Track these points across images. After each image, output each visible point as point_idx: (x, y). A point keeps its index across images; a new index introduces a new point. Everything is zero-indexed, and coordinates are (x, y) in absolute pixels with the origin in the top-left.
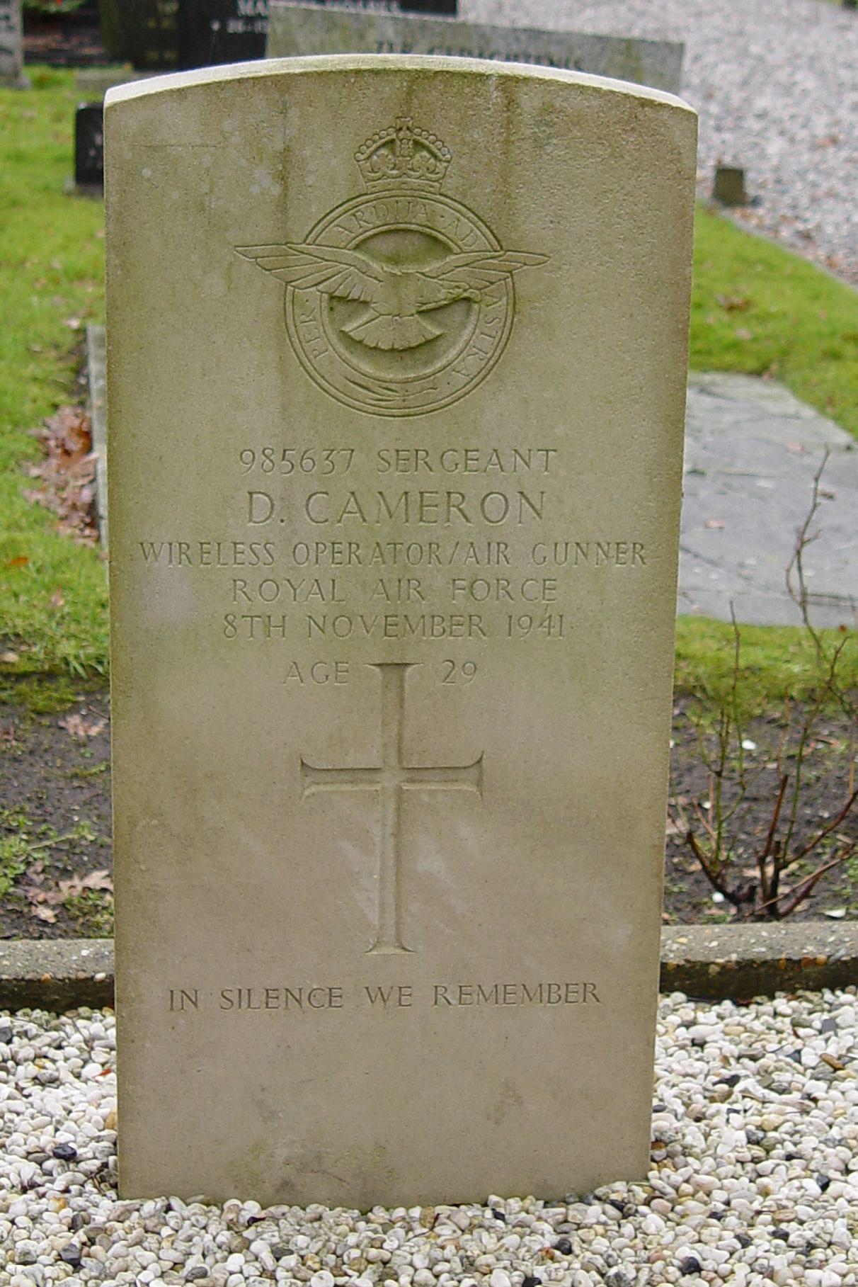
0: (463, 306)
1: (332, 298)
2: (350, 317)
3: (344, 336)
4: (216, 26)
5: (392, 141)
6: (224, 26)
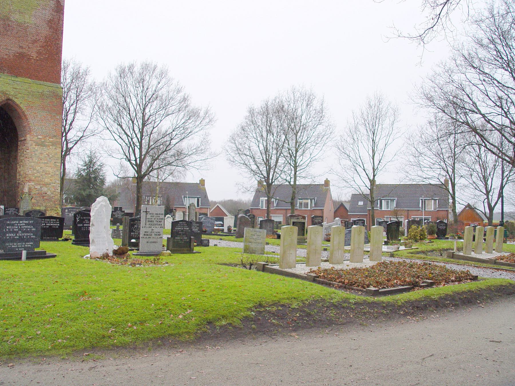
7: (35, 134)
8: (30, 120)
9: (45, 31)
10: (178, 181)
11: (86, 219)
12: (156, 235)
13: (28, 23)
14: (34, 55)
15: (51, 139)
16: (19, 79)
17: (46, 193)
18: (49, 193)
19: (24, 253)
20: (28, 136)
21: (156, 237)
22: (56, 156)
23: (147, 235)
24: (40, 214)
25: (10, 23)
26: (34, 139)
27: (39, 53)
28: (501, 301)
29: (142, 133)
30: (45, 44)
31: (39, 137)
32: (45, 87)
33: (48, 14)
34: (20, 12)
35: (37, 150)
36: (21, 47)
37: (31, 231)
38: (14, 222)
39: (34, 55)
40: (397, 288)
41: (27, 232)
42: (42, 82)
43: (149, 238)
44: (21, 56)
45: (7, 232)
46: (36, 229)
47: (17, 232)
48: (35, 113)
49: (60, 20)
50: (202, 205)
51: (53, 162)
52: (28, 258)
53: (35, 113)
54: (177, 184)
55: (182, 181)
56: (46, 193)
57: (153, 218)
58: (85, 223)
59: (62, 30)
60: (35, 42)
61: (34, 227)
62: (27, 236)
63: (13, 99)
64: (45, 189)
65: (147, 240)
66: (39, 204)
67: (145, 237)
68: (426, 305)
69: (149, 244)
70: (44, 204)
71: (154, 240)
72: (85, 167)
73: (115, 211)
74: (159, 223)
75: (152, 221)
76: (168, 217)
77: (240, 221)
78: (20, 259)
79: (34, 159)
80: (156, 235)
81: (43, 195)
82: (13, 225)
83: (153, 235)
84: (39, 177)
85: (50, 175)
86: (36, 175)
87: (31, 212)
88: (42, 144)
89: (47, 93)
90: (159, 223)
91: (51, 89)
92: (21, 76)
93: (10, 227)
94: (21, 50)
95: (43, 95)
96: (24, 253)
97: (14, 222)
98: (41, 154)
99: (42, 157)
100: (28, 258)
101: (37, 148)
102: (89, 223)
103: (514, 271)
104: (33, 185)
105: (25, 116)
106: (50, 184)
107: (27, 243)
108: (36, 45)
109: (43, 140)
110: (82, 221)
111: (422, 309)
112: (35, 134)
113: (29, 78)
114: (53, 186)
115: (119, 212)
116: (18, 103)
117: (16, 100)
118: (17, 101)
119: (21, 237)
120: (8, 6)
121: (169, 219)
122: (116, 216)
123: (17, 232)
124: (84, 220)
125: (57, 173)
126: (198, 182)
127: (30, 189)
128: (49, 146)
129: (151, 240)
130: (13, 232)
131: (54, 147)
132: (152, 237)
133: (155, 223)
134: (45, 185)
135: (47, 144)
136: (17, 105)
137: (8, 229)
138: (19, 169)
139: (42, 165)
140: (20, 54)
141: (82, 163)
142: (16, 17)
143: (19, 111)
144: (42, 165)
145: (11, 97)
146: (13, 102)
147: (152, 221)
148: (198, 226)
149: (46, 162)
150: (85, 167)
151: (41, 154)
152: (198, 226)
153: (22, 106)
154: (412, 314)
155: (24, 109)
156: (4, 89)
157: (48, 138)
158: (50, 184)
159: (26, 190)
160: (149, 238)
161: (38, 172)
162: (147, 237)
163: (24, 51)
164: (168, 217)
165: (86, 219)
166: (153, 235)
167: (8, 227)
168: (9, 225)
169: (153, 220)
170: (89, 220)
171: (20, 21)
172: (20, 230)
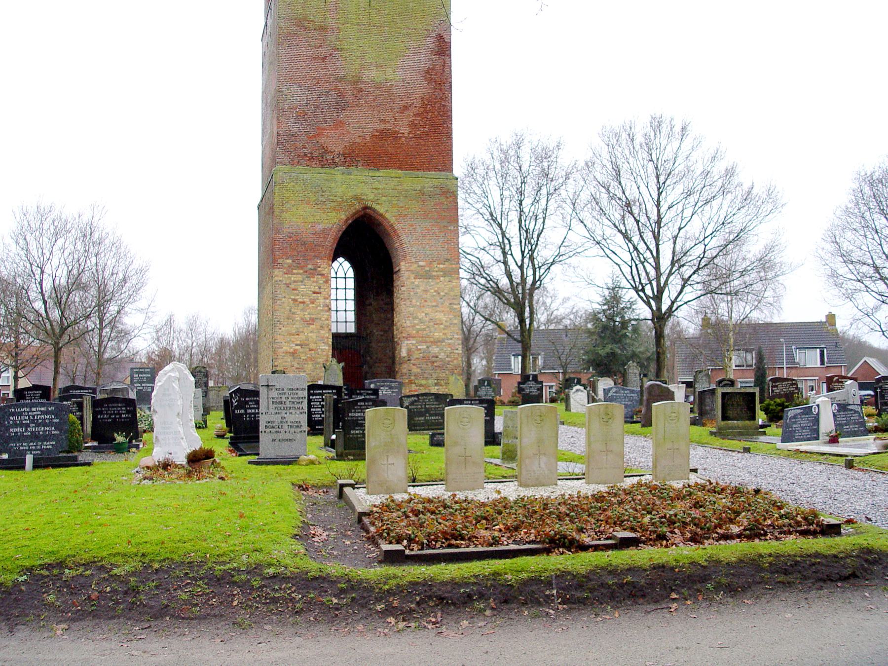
7: (413, 260)
8: (404, 237)
9: (421, 89)
10: (768, 320)
11: (251, 401)
12: (291, 426)
13: (391, 80)
14: (405, 130)
15: (442, 266)
16: (382, 173)
17: (437, 357)
18: (442, 356)
19: (29, 459)
20: (402, 264)
21: (292, 430)
22: (452, 293)
25: (362, 86)
26: (412, 268)
27: (413, 125)
28: (796, 602)
29: (657, 238)
30: (422, 110)
31: (421, 263)
32: (427, 180)
33: (424, 60)
34: (377, 66)
35: (418, 286)
36: (383, 121)
37: (51, 424)
38: (22, 410)
39: (405, 130)
40: (496, 549)
41: (45, 424)
42: (420, 173)
43: (277, 432)
44: (383, 135)
45: (11, 426)
46: (61, 419)
47: (27, 426)
48: (412, 225)
49: (446, 66)
50: (829, 362)
51: (447, 303)
52: (35, 467)
53: (412, 225)
54: (768, 325)
55: (776, 320)
56: (437, 357)
57: (284, 397)
58: (250, 408)
59: (451, 83)
60: (406, 108)
61: (56, 417)
62: (45, 431)
63: (374, 206)
64: (435, 350)
65: (274, 436)
66: (426, 375)
67: (268, 430)
68: (470, 596)
69: (277, 443)
70: (434, 376)
72: (606, 307)
73: (523, 383)
74: (297, 406)
76: (577, 390)
77: (649, 393)
78: (21, 466)
79: (414, 301)
80: (291, 426)
81: (431, 360)
82: (21, 414)
84: (424, 330)
85: (442, 326)
86: (418, 327)
88: (426, 276)
89: (429, 189)
90: (297, 406)
91: (435, 182)
92: (387, 167)
93: (16, 418)
94: (382, 126)
95: (423, 195)
96: (29, 459)
97: (22, 410)
98: (426, 291)
99: (428, 296)
100: (35, 467)
101: (417, 282)
102: (258, 408)
104: (413, 345)
105: (395, 231)
106: (443, 341)
107: (45, 443)
108: (407, 113)
109: (427, 269)
110: (241, 405)
111: (454, 604)
112: (413, 260)
113: (400, 168)
114: (450, 344)
115: (531, 384)
116: (382, 211)
117: (377, 207)
118: (381, 209)
119: (35, 432)
120: (358, 60)
121: (579, 393)
122: (527, 391)
123: (27, 426)
124: (247, 402)
125: (455, 321)
126: (824, 320)
127: (409, 351)
128: (438, 277)
130: (21, 425)
131: (447, 279)
132: (282, 431)
133: (288, 405)
134: (436, 342)
135: (435, 274)
136: (381, 215)
137: (13, 420)
138: (396, 320)
139: (428, 310)
140: (381, 132)
141: (600, 300)
142: (372, 75)
143: (385, 223)
144: (428, 310)
145: (369, 204)
146: (374, 210)
149: (434, 304)
150: (606, 307)
151: (426, 291)
153: (388, 216)
154: (406, 615)
155: (392, 220)
156: (358, 191)
157: (435, 264)
158: (443, 341)
159: (404, 353)
160: (277, 432)
161: (421, 321)
163: (388, 126)
164: (577, 390)
165: (251, 401)
167: (12, 418)
168: (13, 414)
169: (283, 400)
170: (257, 403)
171: (378, 80)
172: (33, 421)
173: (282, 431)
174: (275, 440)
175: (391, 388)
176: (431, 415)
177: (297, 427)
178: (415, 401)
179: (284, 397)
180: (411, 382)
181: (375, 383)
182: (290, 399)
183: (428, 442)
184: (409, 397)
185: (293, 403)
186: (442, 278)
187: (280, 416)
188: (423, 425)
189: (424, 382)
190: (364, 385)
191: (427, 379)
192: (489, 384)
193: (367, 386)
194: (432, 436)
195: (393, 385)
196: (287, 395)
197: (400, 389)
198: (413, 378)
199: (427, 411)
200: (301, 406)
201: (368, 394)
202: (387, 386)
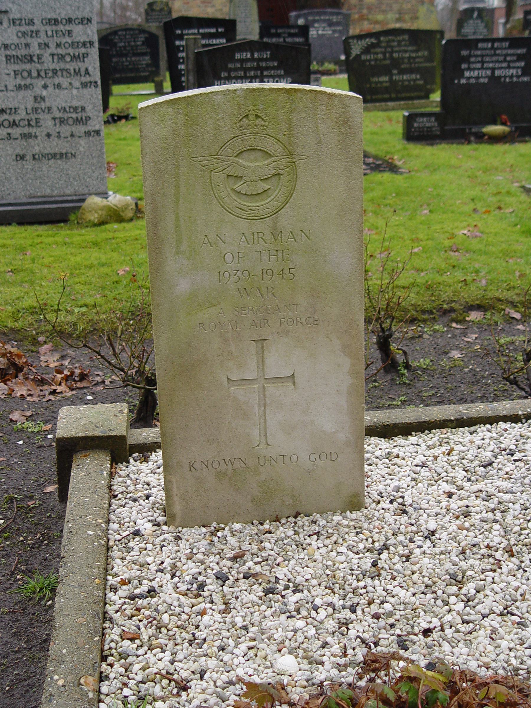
0: (276, 178)
1: (228, 176)
2: (235, 183)
3: (234, 190)
4: (456, 82)
5: (247, 115)
6: (459, 81)
12: (62, 121)
21: (66, 130)
23: (14, 124)
24: (142, 38)
43: (26, 136)
57: (35, 43)
66: (384, 7)
69: (29, 164)
71: (62, 146)
74: (71, 66)
75: (30, 59)
80: (62, 121)
83: (47, 123)
87: (115, 33)
90: (71, 66)
103: (530, 416)
129: (37, 146)
132: (40, 132)
133: (49, 64)
147: (30, 59)
148: (520, 58)
152: (520, 58)
162: (16, 132)
166: (47, 123)
169: (35, 50)
173: (40, 132)
174: (22, 157)
175: (331, 24)
176: (402, 72)
177: (77, 121)
178: (373, 45)
179: (35, 43)
180: (362, 18)
181: (305, 16)
182: (53, 49)
183: (399, 129)
184: (360, 37)
185: (62, 57)
186: (165, 528)
187: (29, 94)
188: (387, 90)
189: (380, 17)
190: (288, 18)
191: (385, 12)
192: (480, 16)
193: (292, 22)
194: (409, 120)
195: (335, 19)
196: (43, 38)
197: (347, 27)
198: (365, 11)
199: (396, 63)
200: (82, 67)
201: (291, 35)
202: (325, 21)
